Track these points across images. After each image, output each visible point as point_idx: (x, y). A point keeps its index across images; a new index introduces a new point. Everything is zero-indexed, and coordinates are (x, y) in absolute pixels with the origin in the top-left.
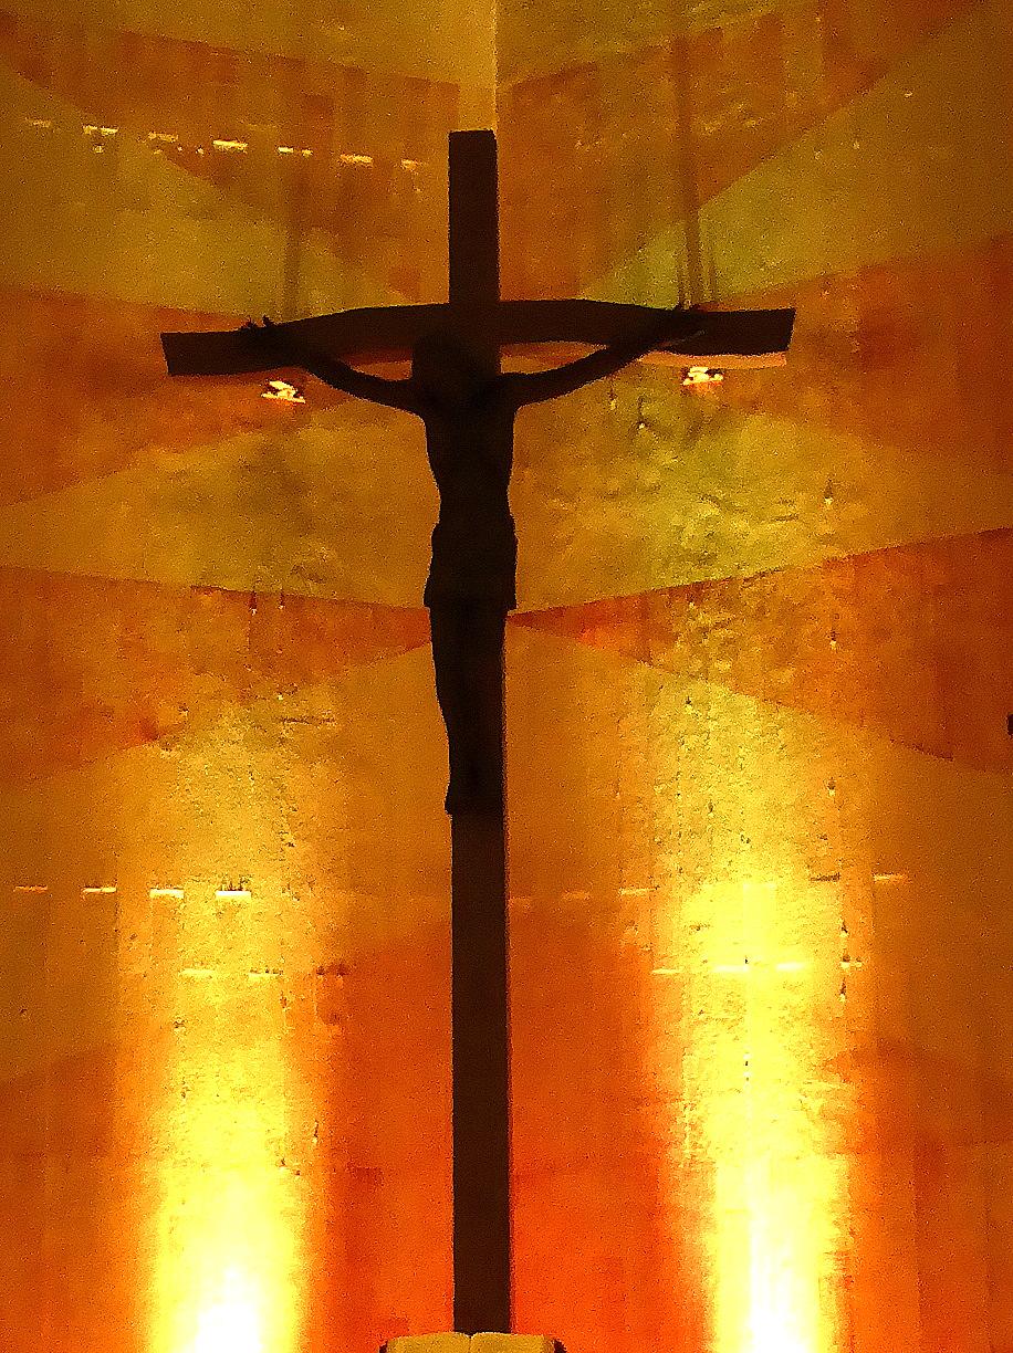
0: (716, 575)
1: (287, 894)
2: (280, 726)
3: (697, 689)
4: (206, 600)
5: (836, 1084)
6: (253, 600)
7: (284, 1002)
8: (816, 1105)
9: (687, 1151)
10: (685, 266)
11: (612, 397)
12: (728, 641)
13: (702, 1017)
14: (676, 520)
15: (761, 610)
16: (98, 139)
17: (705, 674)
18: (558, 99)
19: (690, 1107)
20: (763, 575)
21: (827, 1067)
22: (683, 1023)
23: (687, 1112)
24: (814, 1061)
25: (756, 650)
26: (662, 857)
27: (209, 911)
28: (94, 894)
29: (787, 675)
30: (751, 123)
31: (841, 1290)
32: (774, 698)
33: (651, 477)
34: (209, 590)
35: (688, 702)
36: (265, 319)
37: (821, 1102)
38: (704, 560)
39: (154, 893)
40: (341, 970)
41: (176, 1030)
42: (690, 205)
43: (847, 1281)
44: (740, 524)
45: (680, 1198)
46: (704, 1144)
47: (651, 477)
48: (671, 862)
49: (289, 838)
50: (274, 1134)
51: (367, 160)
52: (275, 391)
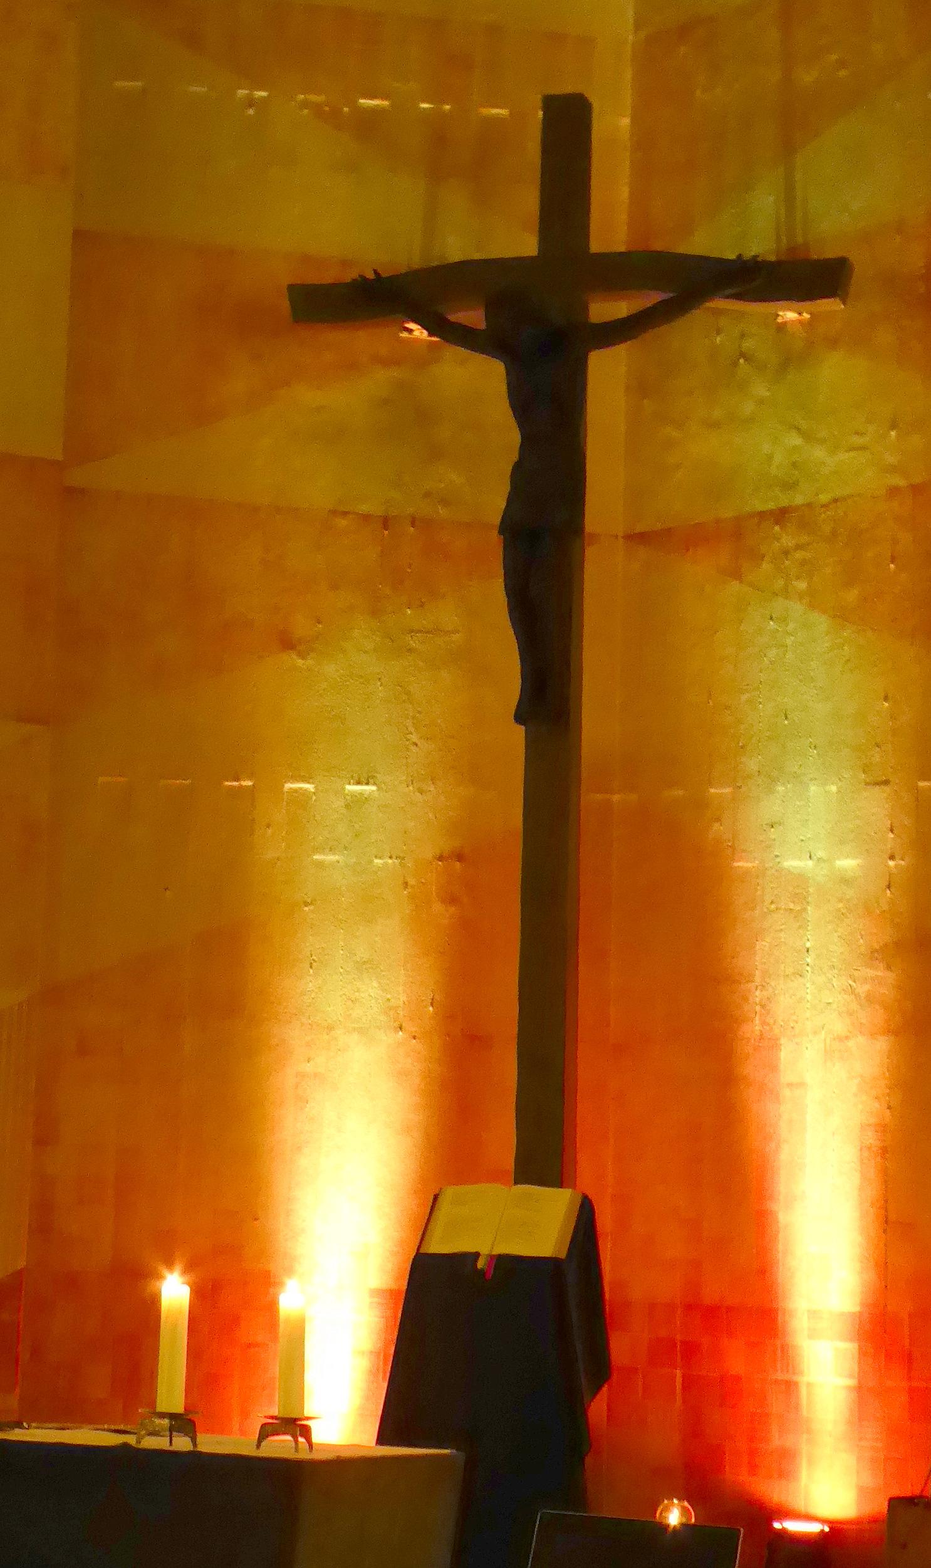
0: (799, 500)
1: (411, 788)
2: (408, 638)
3: (779, 605)
4: (342, 523)
5: (880, 972)
6: (386, 522)
7: (406, 884)
8: (863, 989)
9: (757, 1028)
10: (783, 211)
11: (718, 332)
12: (803, 563)
13: (773, 907)
14: (766, 448)
15: (834, 534)
16: (251, 102)
17: (786, 592)
18: (683, 49)
19: (759, 987)
20: (836, 500)
21: (875, 955)
22: (757, 912)
23: (758, 993)
24: (863, 949)
25: (828, 570)
26: (743, 759)
27: (339, 803)
28: (234, 787)
29: (852, 596)
30: (843, 73)
31: (879, 1159)
32: (842, 616)
33: (748, 408)
34: (345, 514)
35: (771, 618)
36: (375, 272)
37: (867, 987)
38: (789, 486)
39: (289, 786)
40: (460, 857)
41: (306, 909)
42: (788, 148)
43: (884, 1151)
44: (819, 453)
45: (749, 1069)
46: (771, 1021)
47: (748, 408)
48: (752, 764)
49: (414, 738)
50: (393, 1003)
51: (503, 112)
52: (410, 331)
